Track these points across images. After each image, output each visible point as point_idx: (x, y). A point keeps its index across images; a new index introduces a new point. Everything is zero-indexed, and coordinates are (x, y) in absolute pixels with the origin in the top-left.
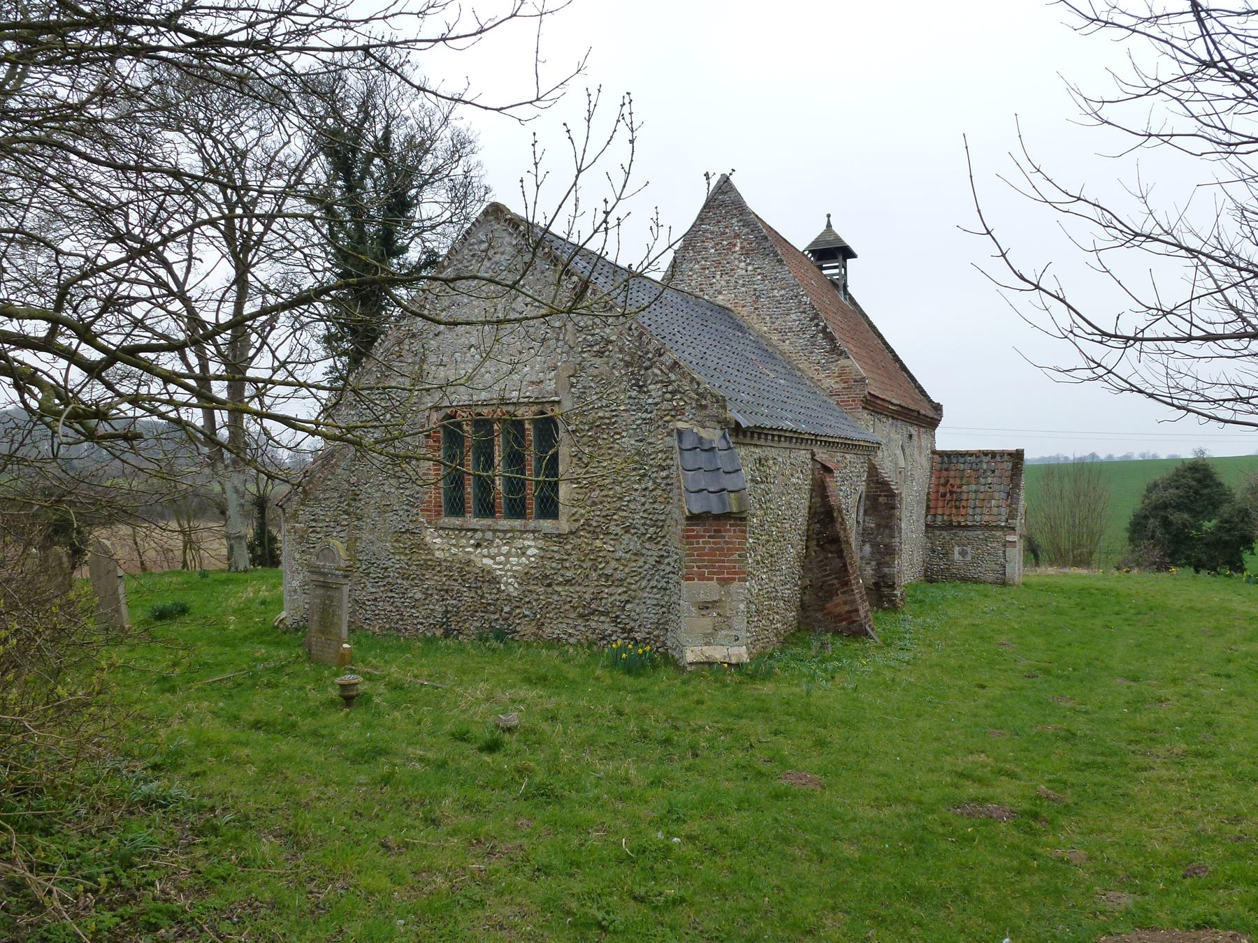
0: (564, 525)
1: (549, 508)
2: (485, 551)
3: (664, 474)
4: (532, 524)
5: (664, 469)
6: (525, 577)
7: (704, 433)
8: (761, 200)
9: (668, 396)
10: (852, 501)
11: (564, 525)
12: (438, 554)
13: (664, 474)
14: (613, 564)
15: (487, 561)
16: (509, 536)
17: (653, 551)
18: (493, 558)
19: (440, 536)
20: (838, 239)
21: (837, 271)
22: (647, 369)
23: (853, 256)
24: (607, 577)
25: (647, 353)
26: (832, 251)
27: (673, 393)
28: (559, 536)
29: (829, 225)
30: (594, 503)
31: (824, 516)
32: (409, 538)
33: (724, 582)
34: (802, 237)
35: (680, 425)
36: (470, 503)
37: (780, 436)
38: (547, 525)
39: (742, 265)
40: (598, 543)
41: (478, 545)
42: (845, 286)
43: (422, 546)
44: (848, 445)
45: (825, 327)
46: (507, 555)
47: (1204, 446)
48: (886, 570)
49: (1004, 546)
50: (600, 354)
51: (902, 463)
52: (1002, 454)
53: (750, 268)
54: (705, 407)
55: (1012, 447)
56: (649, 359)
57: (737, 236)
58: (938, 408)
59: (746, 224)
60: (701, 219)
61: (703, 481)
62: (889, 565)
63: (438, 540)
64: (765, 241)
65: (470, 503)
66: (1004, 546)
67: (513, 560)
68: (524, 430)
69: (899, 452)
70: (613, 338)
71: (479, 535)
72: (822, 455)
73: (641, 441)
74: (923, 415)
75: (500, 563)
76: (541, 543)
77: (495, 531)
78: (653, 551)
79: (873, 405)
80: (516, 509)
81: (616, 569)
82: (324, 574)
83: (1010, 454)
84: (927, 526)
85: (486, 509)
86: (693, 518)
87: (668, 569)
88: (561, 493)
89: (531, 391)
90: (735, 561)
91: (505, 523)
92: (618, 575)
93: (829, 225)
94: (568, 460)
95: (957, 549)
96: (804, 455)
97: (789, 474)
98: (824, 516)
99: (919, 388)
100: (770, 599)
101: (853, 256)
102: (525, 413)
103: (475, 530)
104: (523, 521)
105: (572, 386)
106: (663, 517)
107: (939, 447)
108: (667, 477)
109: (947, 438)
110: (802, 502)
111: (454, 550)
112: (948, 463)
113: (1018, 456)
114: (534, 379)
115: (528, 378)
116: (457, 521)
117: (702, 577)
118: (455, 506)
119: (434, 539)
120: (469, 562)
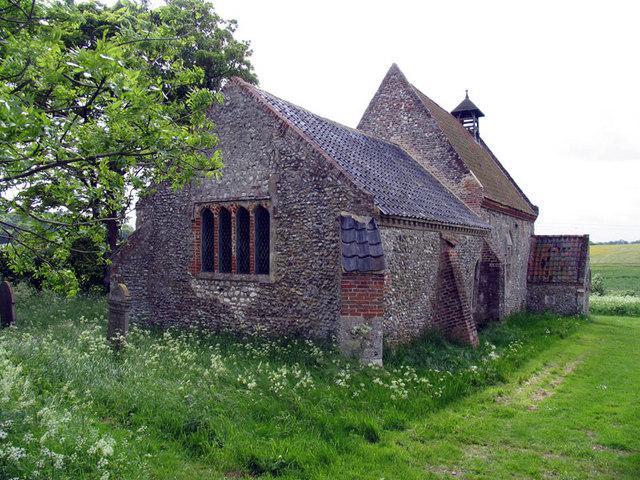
0: (272, 278)
1: (264, 268)
2: (226, 294)
3: (334, 245)
4: (253, 277)
5: (334, 242)
6: (249, 312)
7: (359, 219)
8: (421, 80)
9: (337, 195)
10: (471, 266)
11: (272, 278)
12: (198, 295)
13: (334, 245)
14: (302, 304)
15: (227, 300)
16: (241, 284)
17: (326, 296)
18: (230, 298)
19: (199, 284)
20: (473, 105)
21: (472, 124)
22: (323, 178)
23: (483, 115)
24: (299, 312)
25: (324, 167)
26: (468, 112)
27: (340, 193)
28: (269, 285)
29: (467, 97)
30: (290, 264)
31: (448, 274)
32: (182, 286)
33: (368, 317)
34: (450, 104)
35: (343, 213)
36: (217, 262)
37: (415, 222)
38: (262, 278)
39: (406, 118)
40: (293, 290)
41: (221, 290)
42: (478, 134)
43: (189, 289)
44: (466, 229)
45: (457, 156)
46: (239, 296)
47: (397, 63)
48: (494, 310)
49: (576, 295)
50: (296, 168)
51: (510, 242)
52: (575, 237)
53: (411, 120)
54: (359, 202)
55: (581, 233)
56: (325, 172)
57: (402, 100)
58: (536, 209)
59: (409, 93)
60: (381, 90)
61: (355, 249)
62: (497, 306)
63: (198, 286)
64: (420, 105)
65: (217, 262)
66: (576, 295)
67: (242, 300)
68: (249, 217)
69: (508, 236)
70: (303, 158)
71: (222, 283)
72: (447, 235)
73: (320, 224)
74: (530, 214)
75: (234, 301)
76: (258, 289)
77: (231, 281)
78: (326, 296)
79: (489, 205)
80: (244, 269)
81: (304, 307)
82: (116, 305)
83: (581, 238)
84: (528, 282)
85: (227, 268)
86: (348, 274)
87: (336, 307)
88: (271, 257)
89: (253, 193)
90: (375, 303)
91: (237, 277)
92: (305, 311)
93: (467, 97)
94: (275, 235)
95: (546, 297)
96: (432, 234)
97: (424, 248)
98: (448, 274)
99: (524, 196)
100: (408, 327)
101: (483, 115)
102: (250, 206)
103: (220, 281)
104: (247, 276)
105: (278, 189)
106: (332, 274)
107: (537, 233)
108: (335, 248)
109: (541, 228)
110: (434, 266)
111: (207, 292)
112: (545, 246)
113: (584, 240)
114: (255, 184)
115: (252, 185)
116: (208, 275)
117: (353, 313)
118: (209, 266)
119: (195, 285)
120: (216, 300)
